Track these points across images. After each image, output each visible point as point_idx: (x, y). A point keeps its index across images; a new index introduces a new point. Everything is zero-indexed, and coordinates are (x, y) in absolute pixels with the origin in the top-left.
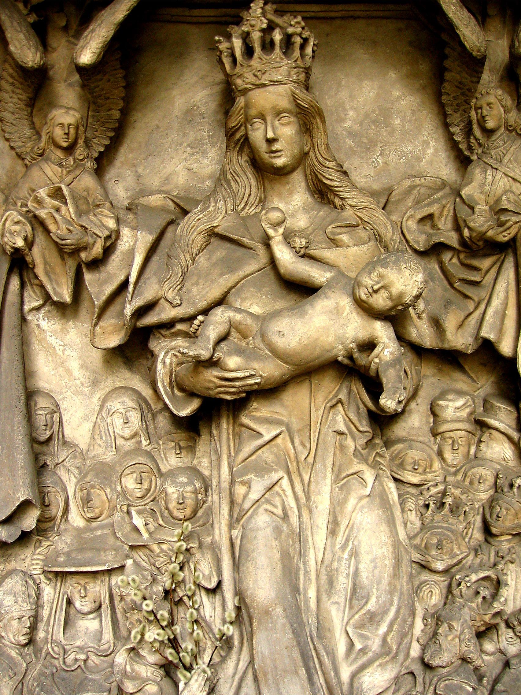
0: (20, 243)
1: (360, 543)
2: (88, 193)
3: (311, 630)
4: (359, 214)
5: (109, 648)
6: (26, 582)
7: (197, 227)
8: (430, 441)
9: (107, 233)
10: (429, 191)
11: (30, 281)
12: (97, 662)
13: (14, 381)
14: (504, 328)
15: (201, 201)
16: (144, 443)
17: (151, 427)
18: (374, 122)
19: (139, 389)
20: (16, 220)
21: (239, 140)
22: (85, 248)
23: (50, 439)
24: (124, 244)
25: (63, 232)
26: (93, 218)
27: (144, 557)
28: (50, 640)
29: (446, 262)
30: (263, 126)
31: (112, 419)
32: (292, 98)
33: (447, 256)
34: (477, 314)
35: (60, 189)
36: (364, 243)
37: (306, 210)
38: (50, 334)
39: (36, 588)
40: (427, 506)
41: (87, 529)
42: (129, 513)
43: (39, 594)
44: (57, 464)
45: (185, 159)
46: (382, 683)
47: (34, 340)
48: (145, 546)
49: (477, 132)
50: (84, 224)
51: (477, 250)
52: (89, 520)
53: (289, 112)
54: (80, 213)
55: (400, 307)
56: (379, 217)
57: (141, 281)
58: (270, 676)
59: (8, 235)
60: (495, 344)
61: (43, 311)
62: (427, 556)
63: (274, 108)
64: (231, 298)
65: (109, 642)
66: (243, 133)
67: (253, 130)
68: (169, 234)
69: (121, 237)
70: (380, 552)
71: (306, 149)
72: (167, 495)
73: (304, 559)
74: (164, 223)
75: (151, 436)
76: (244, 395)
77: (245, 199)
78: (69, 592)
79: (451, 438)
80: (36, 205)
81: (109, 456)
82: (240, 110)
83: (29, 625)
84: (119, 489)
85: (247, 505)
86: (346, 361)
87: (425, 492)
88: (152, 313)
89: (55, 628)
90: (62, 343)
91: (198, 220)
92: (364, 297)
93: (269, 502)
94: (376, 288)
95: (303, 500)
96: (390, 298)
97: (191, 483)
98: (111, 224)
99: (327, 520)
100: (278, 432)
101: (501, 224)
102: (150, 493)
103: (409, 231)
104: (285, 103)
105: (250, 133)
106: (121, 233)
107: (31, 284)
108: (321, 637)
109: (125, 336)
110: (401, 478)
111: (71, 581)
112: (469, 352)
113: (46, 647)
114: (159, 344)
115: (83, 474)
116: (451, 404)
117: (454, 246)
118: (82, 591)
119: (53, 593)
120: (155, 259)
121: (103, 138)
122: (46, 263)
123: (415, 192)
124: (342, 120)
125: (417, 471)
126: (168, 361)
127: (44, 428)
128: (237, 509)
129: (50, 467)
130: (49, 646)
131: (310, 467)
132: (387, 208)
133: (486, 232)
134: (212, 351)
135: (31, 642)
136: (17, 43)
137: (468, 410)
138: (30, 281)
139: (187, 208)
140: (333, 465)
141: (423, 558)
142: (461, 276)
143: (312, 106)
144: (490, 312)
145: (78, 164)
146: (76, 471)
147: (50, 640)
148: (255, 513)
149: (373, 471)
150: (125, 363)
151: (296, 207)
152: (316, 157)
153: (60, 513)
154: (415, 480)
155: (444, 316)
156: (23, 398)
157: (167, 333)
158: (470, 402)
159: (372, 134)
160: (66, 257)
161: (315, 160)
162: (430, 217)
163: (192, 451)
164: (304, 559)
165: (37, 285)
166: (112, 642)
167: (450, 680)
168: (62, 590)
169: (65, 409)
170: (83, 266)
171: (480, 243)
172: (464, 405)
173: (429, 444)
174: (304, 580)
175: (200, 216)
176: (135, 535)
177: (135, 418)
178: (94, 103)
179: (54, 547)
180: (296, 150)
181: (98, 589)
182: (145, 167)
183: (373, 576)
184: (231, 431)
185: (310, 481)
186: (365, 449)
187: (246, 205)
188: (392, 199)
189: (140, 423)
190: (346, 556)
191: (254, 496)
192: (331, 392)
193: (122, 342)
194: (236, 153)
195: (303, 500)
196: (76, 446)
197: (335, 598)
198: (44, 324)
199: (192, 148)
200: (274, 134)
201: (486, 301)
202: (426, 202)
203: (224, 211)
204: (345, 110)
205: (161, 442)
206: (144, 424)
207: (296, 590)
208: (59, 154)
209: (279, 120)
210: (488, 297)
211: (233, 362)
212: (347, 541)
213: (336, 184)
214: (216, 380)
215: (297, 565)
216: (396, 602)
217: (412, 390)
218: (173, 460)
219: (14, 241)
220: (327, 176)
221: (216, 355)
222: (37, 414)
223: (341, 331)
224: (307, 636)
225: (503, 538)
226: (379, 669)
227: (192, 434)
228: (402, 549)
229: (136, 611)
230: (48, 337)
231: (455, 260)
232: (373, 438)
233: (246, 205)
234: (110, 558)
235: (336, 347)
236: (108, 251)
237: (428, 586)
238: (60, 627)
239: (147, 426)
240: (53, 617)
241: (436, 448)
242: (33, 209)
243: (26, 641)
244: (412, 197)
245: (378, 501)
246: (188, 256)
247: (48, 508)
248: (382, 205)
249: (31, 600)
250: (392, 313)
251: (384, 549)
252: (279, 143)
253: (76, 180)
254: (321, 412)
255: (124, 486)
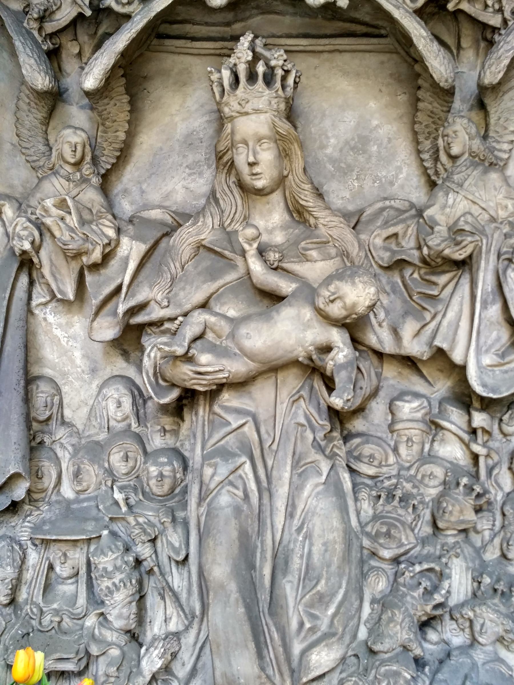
0: (27, 246)
1: (313, 527)
2: (93, 205)
3: (263, 606)
4: (329, 232)
5: (82, 612)
6: (12, 547)
7: (187, 239)
8: (387, 437)
9: (106, 241)
10: (396, 213)
11: (39, 281)
12: (70, 624)
13: (15, 367)
14: (457, 338)
15: (192, 216)
16: (134, 425)
17: (142, 411)
18: (352, 149)
19: (133, 378)
20: (25, 225)
21: (227, 163)
22: (86, 253)
23: (49, 418)
24: (123, 250)
25: (66, 237)
26: (94, 227)
27: (122, 529)
28: (29, 602)
29: (407, 278)
30: (246, 151)
31: (107, 404)
32: (272, 125)
33: (408, 272)
34: (432, 325)
35: (65, 200)
36: (332, 258)
37: (284, 227)
38: (55, 326)
39: (21, 553)
40: (379, 497)
41: (77, 501)
42: (112, 488)
43: (25, 558)
44: (54, 441)
45: (184, 178)
46: (328, 663)
47: (40, 331)
48: (123, 519)
49: (443, 157)
50: (85, 232)
51: (436, 267)
52: (78, 492)
53: (269, 138)
54: (83, 222)
55: (354, 316)
56: (348, 235)
57: (136, 282)
58: (222, 648)
59: (16, 238)
60: (448, 353)
61: (50, 306)
62: (376, 544)
63: (256, 134)
64: (212, 303)
65: (83, 606)
66: (230, 157)
67: (237, 154)
68: (163, 244)
69: (121, 245)
70: (331, 537)
71: (285, 173)
72: (148, 473)
73: (262, 538)
74: (159, 235)
75: (141, 419)
76: (214, 387)
77: (231, 216)
78: (51, 558)
79: (406, 435)
80: (43, 214)
81: (102, 436)
82: (227, 136)
83: (10, 587)
84: (106, 465)
85: (212, 486)
86: (306, 362)
87: (378, 484)
88: (143, 312)
89: (36, 591)
90: (67, 335)
91: (188, 233)
92: (322, 306)
93: (231, 484)
94: (332, 298)
95: (265, 484)
96: (345, 307)
97: (170, 463)
98: (111, 233)
99: (286, 504)
100: (244, 421)
101: (458, 244)
102: (135, 470)
103: (375, 248)
104: (264, 130)
105: (235, 156)
106: (121, 242)
107: (39, 283)
108: (272, 612)
109: (119, 331)
110: (358, 469)
111: (54, 547)
112: (425, 358)
113: (26, 608)
114: (149, 339)
115: (76, 450)
116: (407, 405)
117: (415, 262)
118: (62, 558)
119: (37, 558)
120: (149, 265)
121: (110, 157)
122: (52, 264)
123: (385, 213)
124: (323, 147)
125: (373, 464)
126: (152, 355)
127: (43, 409)
128: (204, 488)
129: (47, 444)
130: (28, 607)
131: (274, 454)
132: (358, 227)
133: (443, 251)
134: (187, 348)
135: (12, 602)
136: (28, 67)
137: (423, 411)
138: (39, 281)
139: (181, 222)
140: (294, 453)
141: (373, 546)
142: (419, 290)
143: (290, 134)
144: (445, 323)
145: (84, 180)
146: (70, 448)
147: (29, 602)
148: (218, 493)
149: (329, 461)
150: (122, 355)
151: (275, 225)
152: (294, 180)
153: (52, 486)
154: (371, 471)
155: (401, 325)
156: (22, 382)
157: (157, 330)
158: (426, 404)
159: (350, 159)
160: (69, 259)
161: (293, 183)
162: (395, 235)
163: (175, 434)
164: (262, 538)
165: (44, 283)
166: (85, 606)
167: (389, 665)
168: (45, 556)
169: (66, 393)
170: (85, 268)
171: (439, 260)
172: (419, 406)
173: (386, 439)
174: (261, 558)
175: (190, 230)
176: (115, 508)
177: (127, 402)
178: (103, 125)
179: (43, 516)
180: (275, 173)
181: (77, 556)
182: (149, 184)
183: (324, 558)
184: (206, 418)
185: (272, 467)
186: (324, 440)
187: (232, 221)
188: (363, 218)
189: (131, 408)
190: (301, 539)
191: (217, 479)
192: (294, 388)
193: (117, 336)
194: (224, 175)
195: (265, 484)
196: (73, 426)
197: (289, 578)
198: (51, 318)
199: (190, 169)
200: (255, 158)
201: (442, 313)
202: (392, 222)
203: (211, 226)
204: (328, 138)
205: (149, 425)
206: (135, 409)
207: (251, 566)
208: (69, 169)
209: (260, 146)
210: (444, 309)
211: (204, 358)
212: (303, 524)
213: (311, 204)
214: (190, 373)
215: (255, 543)
216: (344, 585)
217: (368, 390)
218: (158, 441)
219: (21, 244)
220: (303, 197)
221: (191, 351)
222: (38, 397)
223: (302, 335)
224: (259, 612)
225: (449, 532)
226: (326, 649)
227: (176, 419)
228: (353, 535)
229: (106, 579)
230: (54, 330)
231: (416, 275)
232: (331, 431)
233: (232, 221)
234: (90, 528)
235: (296, 349)
236: (106, 257)
237: (376, 573)
238: (39, 590)
239: (138, 410)
240: (34, 581)
241: (392, 443)
242: (40, 217)
243: (8, 601)
244: (382, 218)
245: (332, 488)
246: (178, 265)
247: (40, 481)
248: (352, 225)
249: (15, 564)
250: (348, 321)
251: (335, 534)
252: (260, 166)
253: (82, 193)
254: (285, 405)
255: (111, 463)
